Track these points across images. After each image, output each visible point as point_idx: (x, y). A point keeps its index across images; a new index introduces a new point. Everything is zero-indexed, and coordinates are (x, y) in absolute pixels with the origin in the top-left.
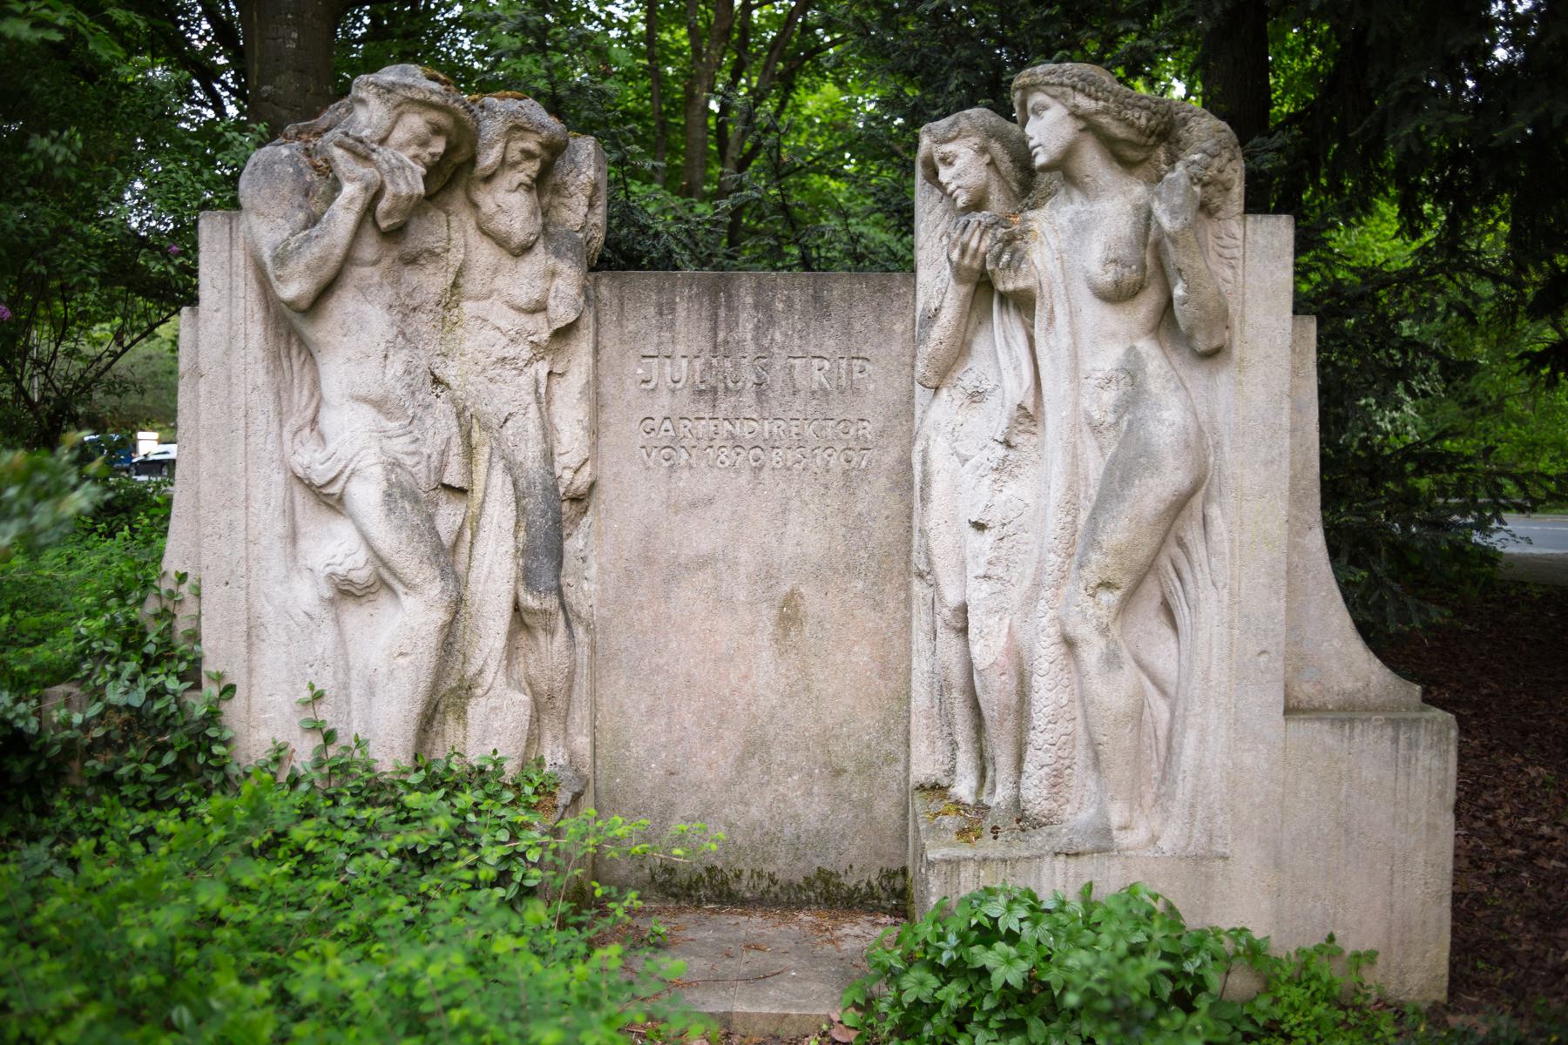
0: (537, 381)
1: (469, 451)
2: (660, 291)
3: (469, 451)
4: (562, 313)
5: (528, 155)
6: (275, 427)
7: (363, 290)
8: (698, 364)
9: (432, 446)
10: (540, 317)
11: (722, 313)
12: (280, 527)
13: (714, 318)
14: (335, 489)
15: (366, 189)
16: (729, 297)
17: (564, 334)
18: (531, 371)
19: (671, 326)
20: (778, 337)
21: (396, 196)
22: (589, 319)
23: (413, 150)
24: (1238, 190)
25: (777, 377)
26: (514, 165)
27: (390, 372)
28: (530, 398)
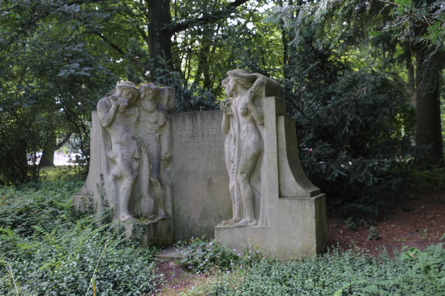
0: (156, 137)
1: (140, 151)
2: (183, 116)
3: (140, 151)
4: (161, 123)
5: (150, 94)
6: (104, 149)
7: (117, 123)
8: (191, 131)
9: (132, 151)
10: (156, 124)
11: (194, 120)
12: (106, 166)
13: (193, 121)
14: (114, 159)
15: (116, 106)
16: (196, 117)
17: (161, 127)
18: (155, 135)
19: (185, 124)
20: (205, 124)
21: (122, 106)
22: (168, 123)
23: (125, 97)
24: (264, 92)
25: (205, 133)
26: (148, 96)
27: (123, 137)
28: (155, 140)
